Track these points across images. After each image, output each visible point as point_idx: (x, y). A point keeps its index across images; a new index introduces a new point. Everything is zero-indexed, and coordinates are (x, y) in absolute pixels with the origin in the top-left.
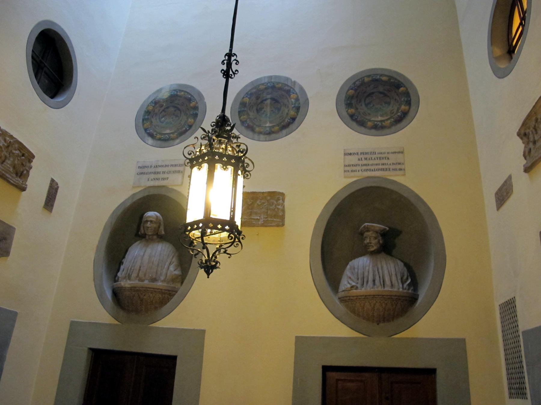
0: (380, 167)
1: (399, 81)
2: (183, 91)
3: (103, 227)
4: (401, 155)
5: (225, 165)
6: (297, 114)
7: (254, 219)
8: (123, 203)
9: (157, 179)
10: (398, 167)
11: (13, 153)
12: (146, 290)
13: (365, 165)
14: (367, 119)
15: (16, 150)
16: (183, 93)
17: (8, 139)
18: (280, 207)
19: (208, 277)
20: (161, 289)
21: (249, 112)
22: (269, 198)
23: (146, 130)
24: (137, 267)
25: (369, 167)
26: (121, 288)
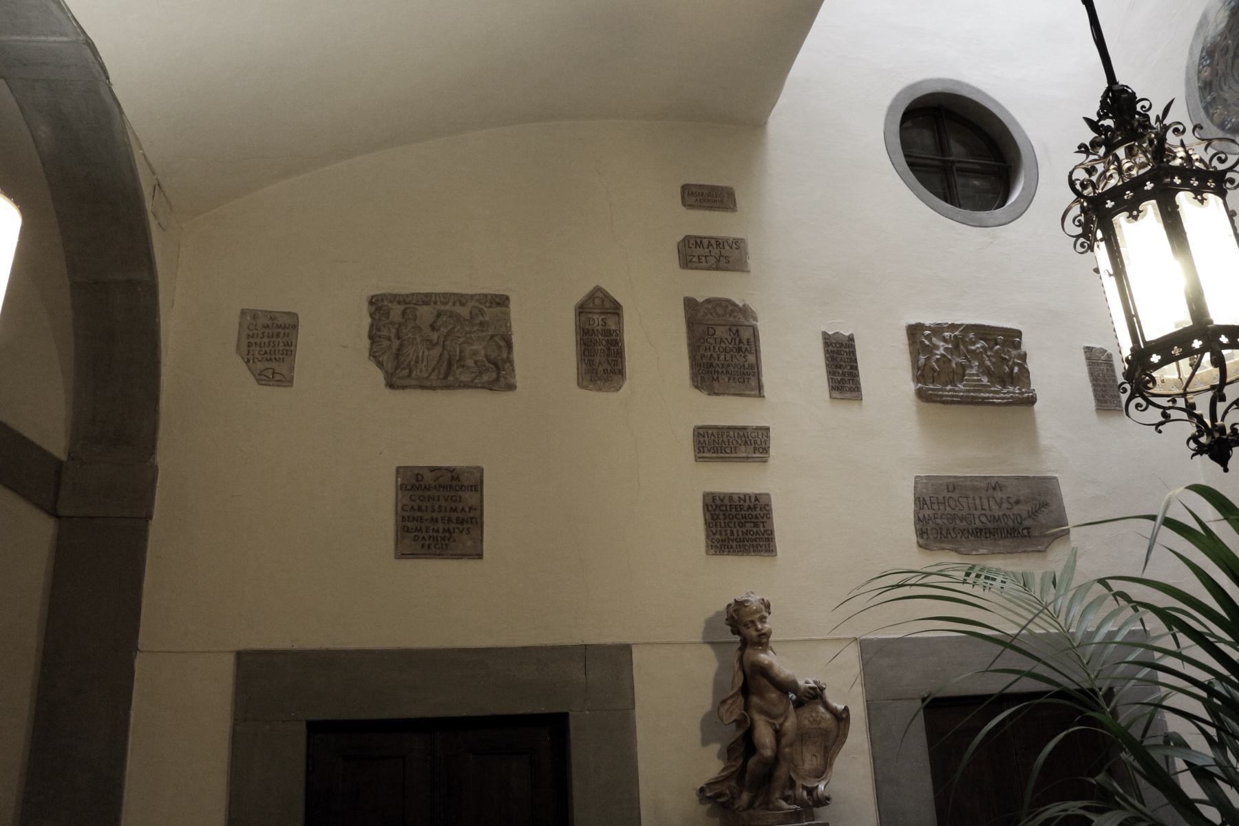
5: (1133, 209)
11: (973, 351)
15: (974, 344)
17: (947, 334)
19: (1226, 470)
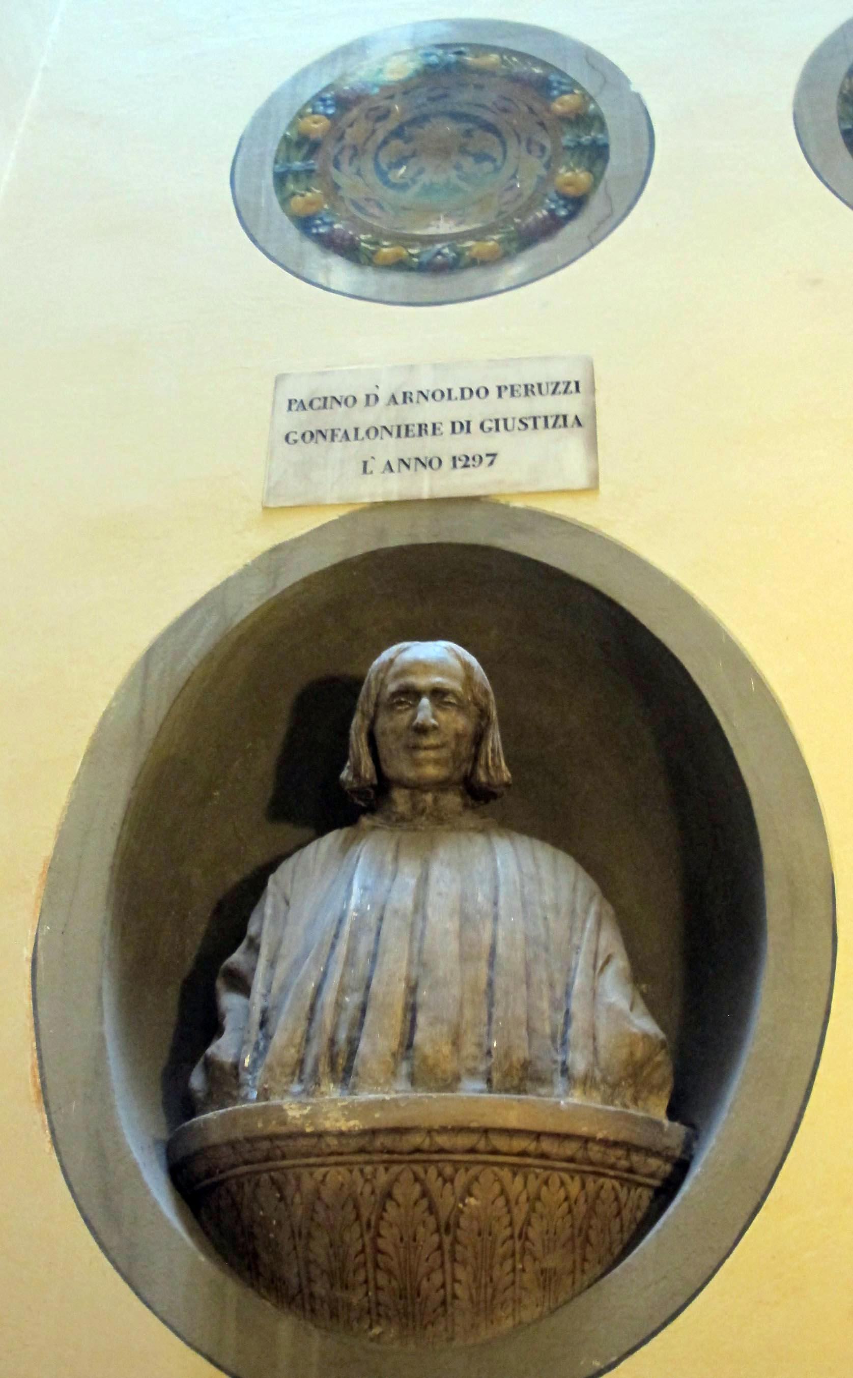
2: (494, 49)
3: (82, 745)
9: (426, 464)
12: (484, 1143)
16: (494, 58)
20: (586, 1140)
23: (305, 223)
24: (390, 989)
26: (277, 1149)
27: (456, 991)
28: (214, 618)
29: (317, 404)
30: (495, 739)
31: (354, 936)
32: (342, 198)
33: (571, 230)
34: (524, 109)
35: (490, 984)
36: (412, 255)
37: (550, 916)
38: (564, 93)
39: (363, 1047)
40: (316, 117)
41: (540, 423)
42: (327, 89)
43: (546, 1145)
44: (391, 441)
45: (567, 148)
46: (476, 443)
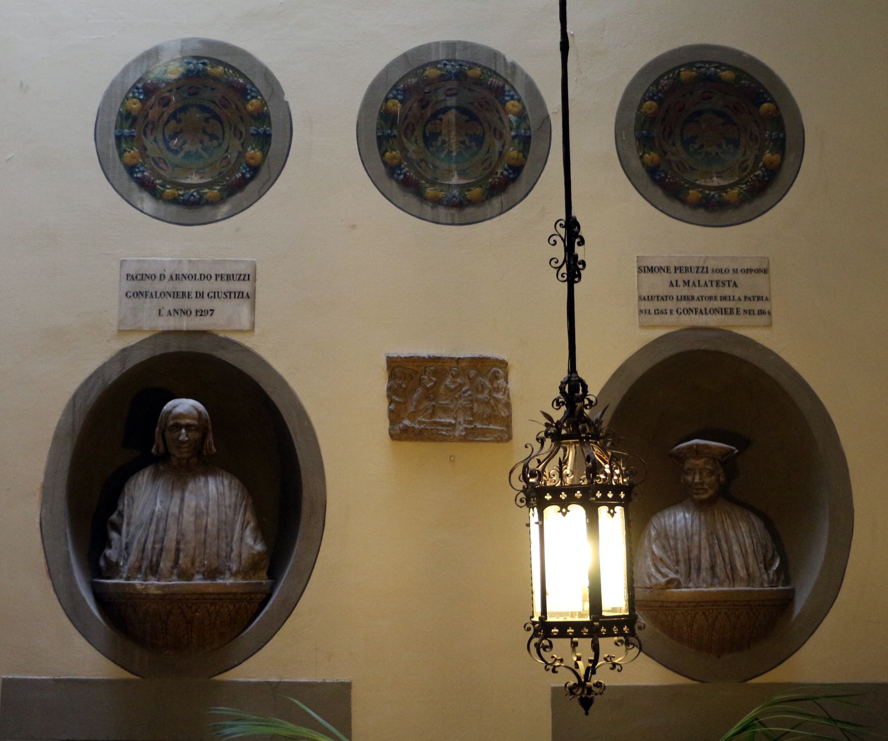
0: (718, 304)
1: (760, 85)
2: (220, 63)
4: (762, 275)
6: (525, 157)
7: (442, 424)
8: (98, 373)
9: (185, 312)
10: (757, 306)
12: (201, 596)
13: (686, 298)
14: (687, 182)
16: (220, 69)
18: (500, 396)
20: (235, 594)
21: (405, 140)
22: (473, 373)
23: (131, 170)
24: (172, 535)
25: (693, 304)
26: (132, 597)
27: (193, 544)
28: (100, 381)
29: (139, 277)
30: (210, 438)
31: (158, 521)
32: (148, 156)
33: (252, 187)
34: (234, 107)
35: (205, 540)
36: (180, 195)
37: (228, 510)
38: (253, 97)
39: (162, 565)
40: (135, 100)
41: (233, 295)
42: (139, 81)
43: (221, 596)
44: (170, 300)
45: (252, 135)
46: (206, 304)
